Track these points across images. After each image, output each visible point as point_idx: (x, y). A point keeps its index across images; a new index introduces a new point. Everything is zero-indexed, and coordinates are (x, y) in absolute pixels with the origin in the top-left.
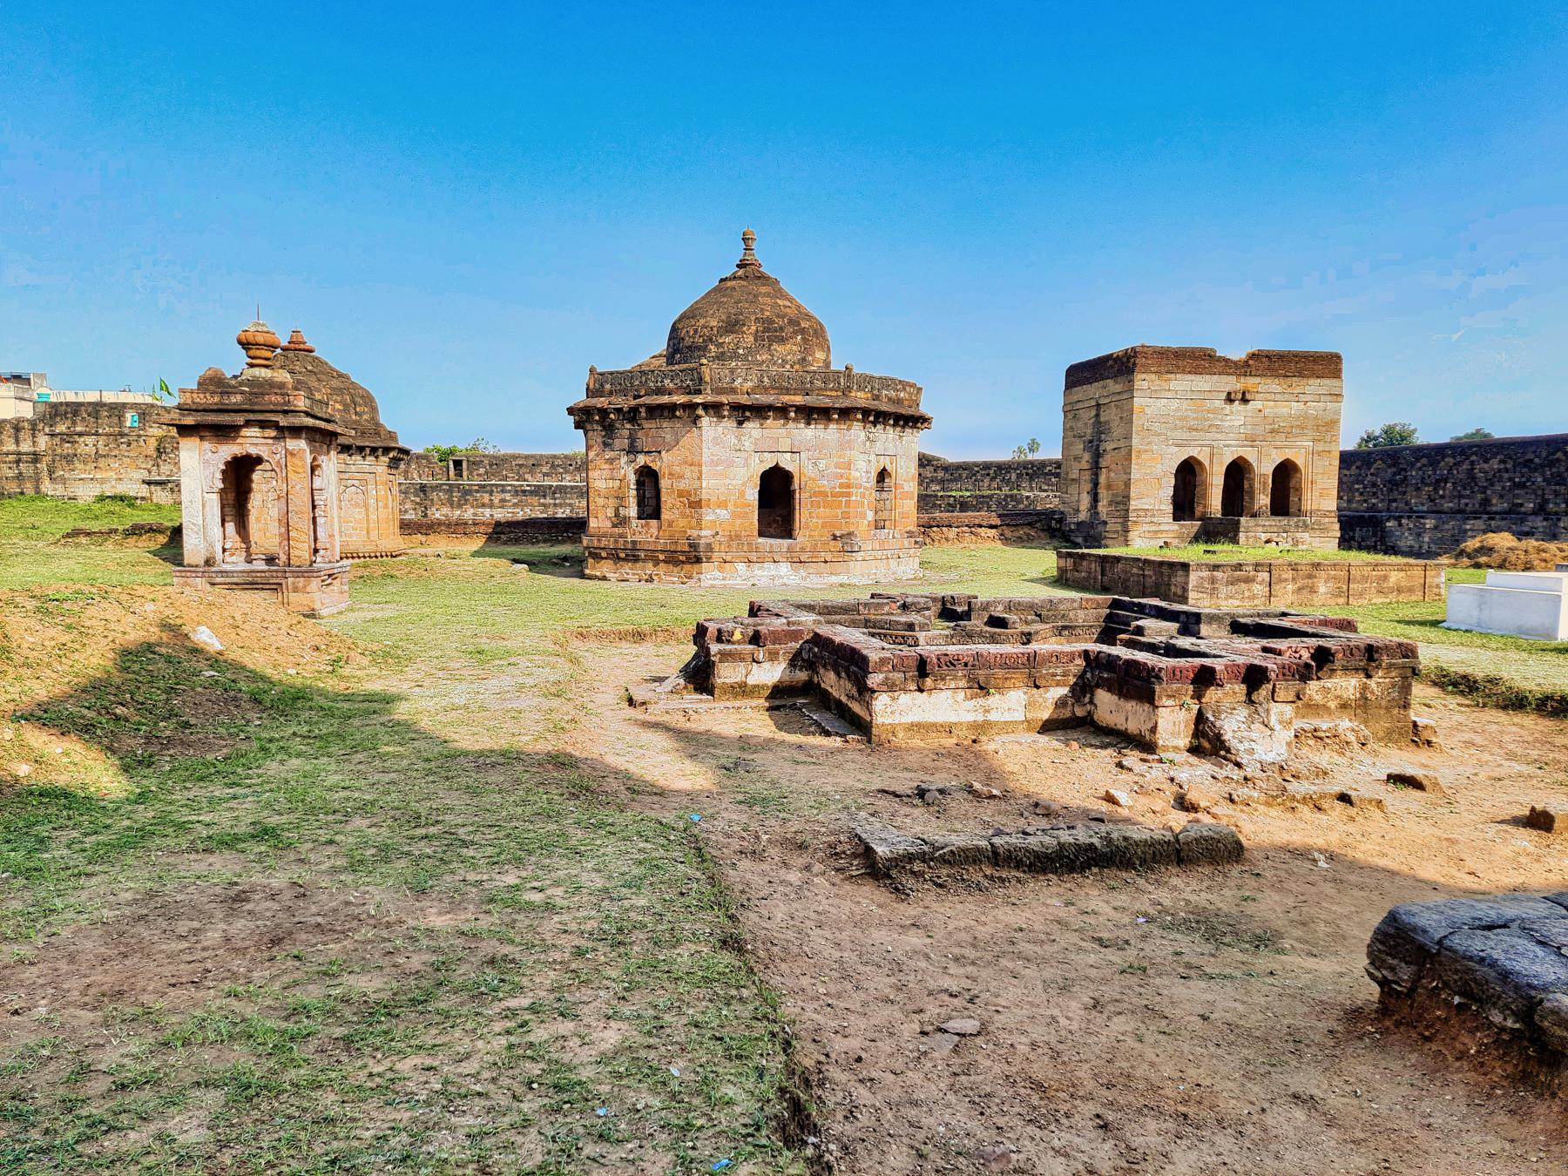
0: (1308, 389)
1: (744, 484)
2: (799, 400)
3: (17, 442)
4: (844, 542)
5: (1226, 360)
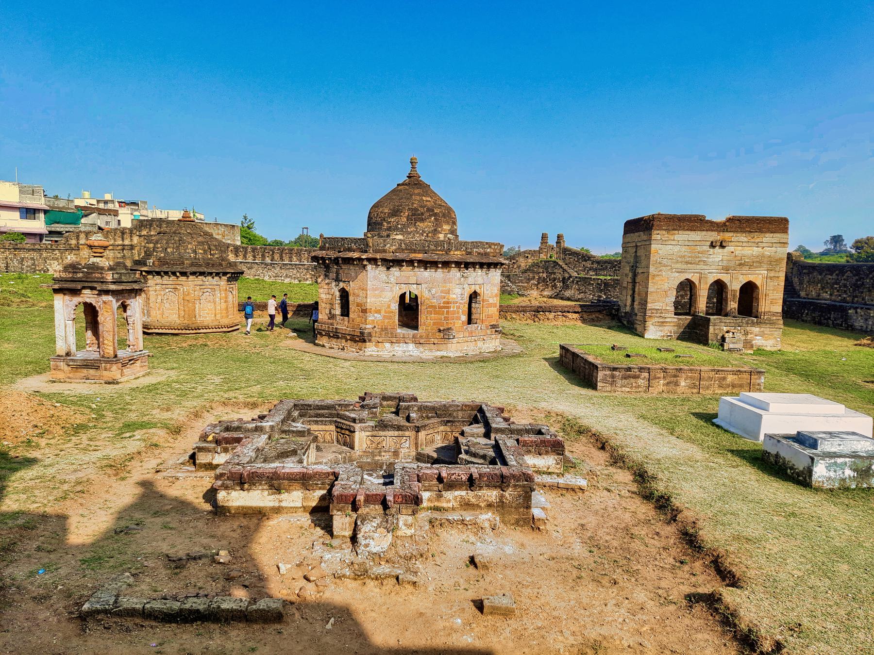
0: (765, 240)
2: (420, 256)
3: (123, 240)
4: (445, 333)
5: (711, 222)
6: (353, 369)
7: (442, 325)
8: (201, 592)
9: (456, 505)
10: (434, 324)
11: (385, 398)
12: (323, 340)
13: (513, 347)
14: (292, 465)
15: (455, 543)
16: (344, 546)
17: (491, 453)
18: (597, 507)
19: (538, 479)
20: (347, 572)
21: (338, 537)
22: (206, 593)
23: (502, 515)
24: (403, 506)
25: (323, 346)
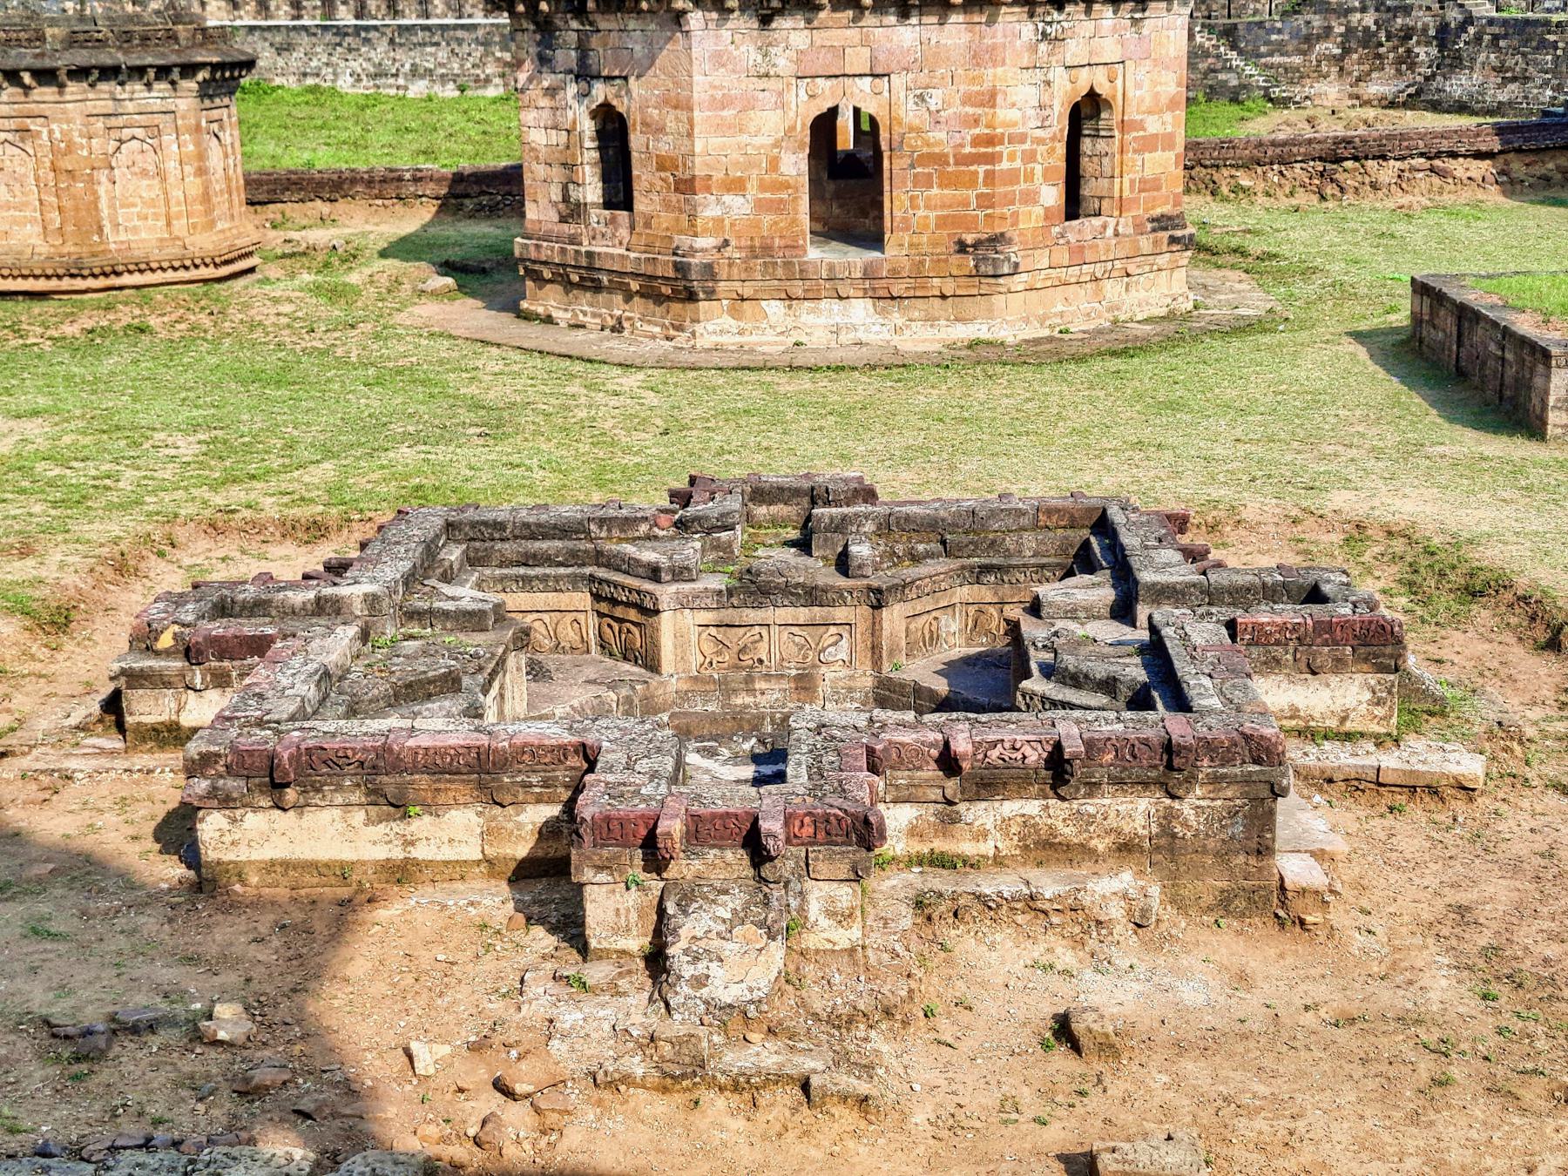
1: (777, 144)
4: (982, 257)
6: (651, 398)
7: (970, 224)
8: (160, 1135)
9: (1007, 847)
10: (942, 222)
11: (761, 494)
12: (547, 300)
13: (1241, 295)
14: (439, 723)
15: (1008, 971)
16: (623, 984)
17: (1135, 671)
18: (1519, 848)
19: (1298, 753)
20: (637, 1066)
21: (603, 955)
22: (176, 1135)
23: (1172, 880)
24: (819, 853)
25: (549, 320)
